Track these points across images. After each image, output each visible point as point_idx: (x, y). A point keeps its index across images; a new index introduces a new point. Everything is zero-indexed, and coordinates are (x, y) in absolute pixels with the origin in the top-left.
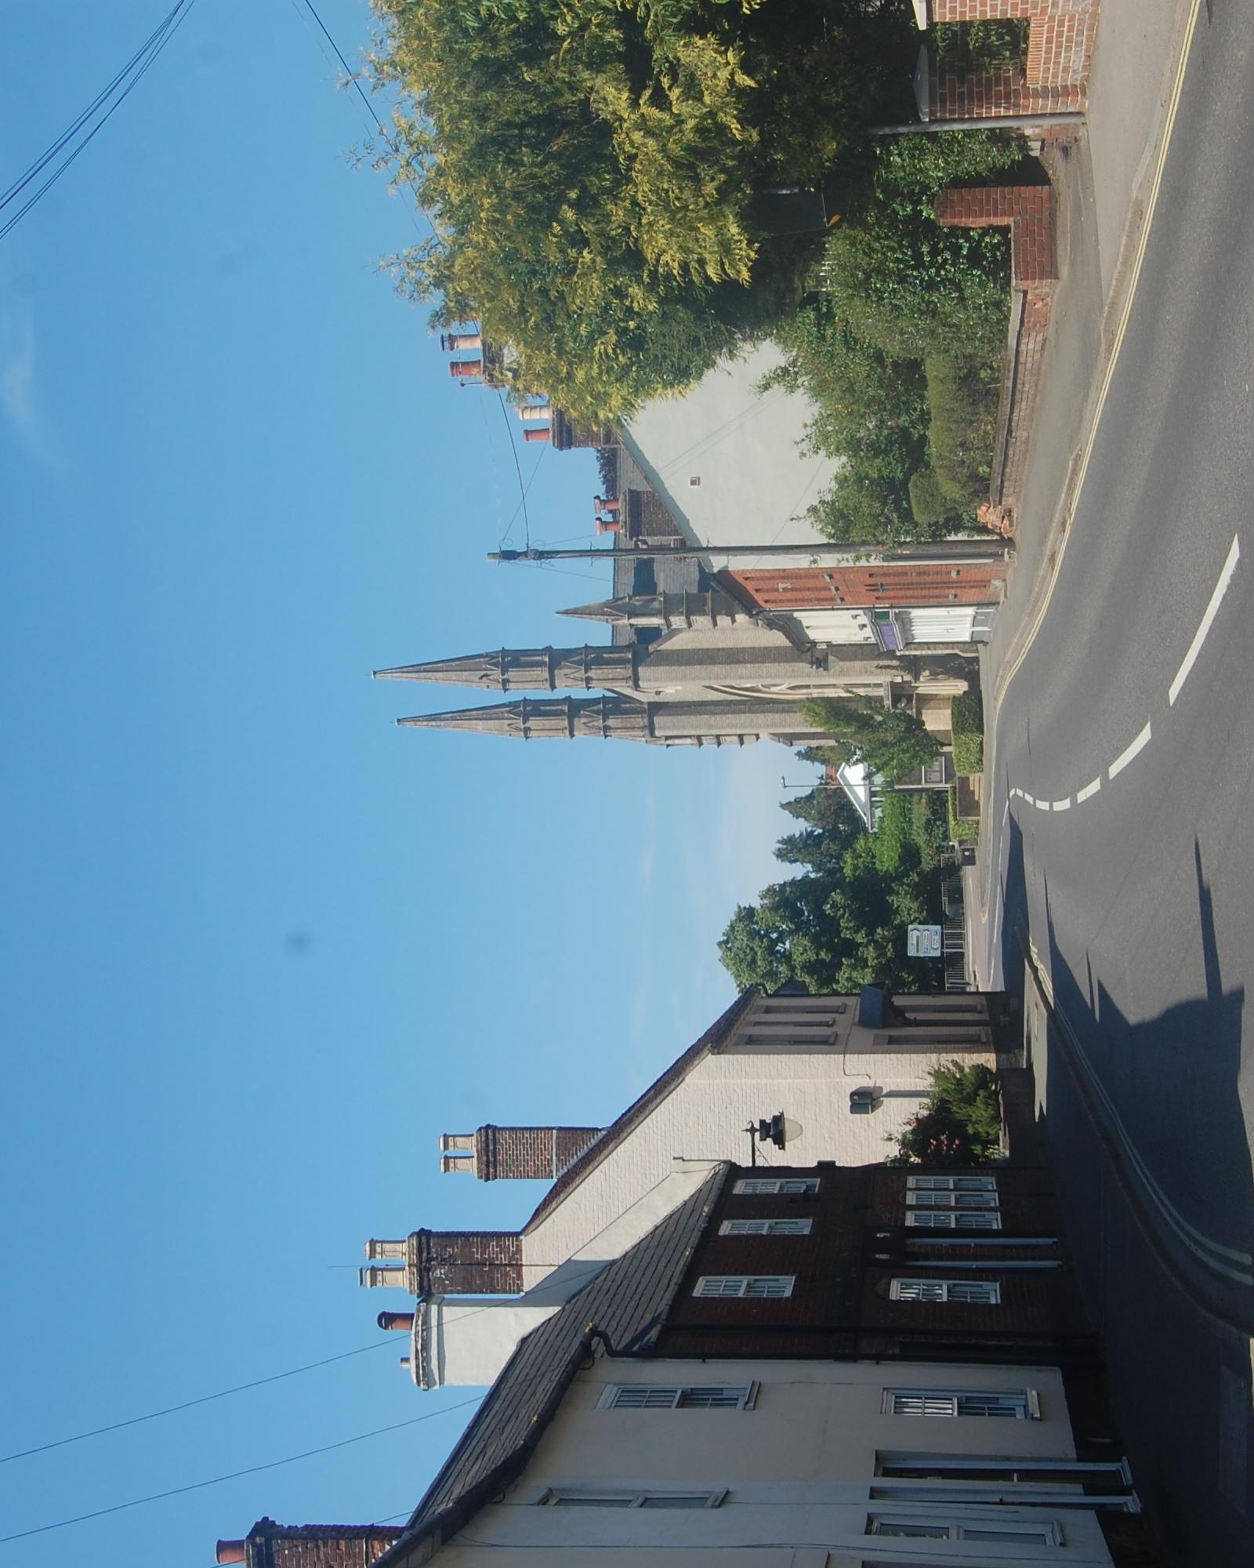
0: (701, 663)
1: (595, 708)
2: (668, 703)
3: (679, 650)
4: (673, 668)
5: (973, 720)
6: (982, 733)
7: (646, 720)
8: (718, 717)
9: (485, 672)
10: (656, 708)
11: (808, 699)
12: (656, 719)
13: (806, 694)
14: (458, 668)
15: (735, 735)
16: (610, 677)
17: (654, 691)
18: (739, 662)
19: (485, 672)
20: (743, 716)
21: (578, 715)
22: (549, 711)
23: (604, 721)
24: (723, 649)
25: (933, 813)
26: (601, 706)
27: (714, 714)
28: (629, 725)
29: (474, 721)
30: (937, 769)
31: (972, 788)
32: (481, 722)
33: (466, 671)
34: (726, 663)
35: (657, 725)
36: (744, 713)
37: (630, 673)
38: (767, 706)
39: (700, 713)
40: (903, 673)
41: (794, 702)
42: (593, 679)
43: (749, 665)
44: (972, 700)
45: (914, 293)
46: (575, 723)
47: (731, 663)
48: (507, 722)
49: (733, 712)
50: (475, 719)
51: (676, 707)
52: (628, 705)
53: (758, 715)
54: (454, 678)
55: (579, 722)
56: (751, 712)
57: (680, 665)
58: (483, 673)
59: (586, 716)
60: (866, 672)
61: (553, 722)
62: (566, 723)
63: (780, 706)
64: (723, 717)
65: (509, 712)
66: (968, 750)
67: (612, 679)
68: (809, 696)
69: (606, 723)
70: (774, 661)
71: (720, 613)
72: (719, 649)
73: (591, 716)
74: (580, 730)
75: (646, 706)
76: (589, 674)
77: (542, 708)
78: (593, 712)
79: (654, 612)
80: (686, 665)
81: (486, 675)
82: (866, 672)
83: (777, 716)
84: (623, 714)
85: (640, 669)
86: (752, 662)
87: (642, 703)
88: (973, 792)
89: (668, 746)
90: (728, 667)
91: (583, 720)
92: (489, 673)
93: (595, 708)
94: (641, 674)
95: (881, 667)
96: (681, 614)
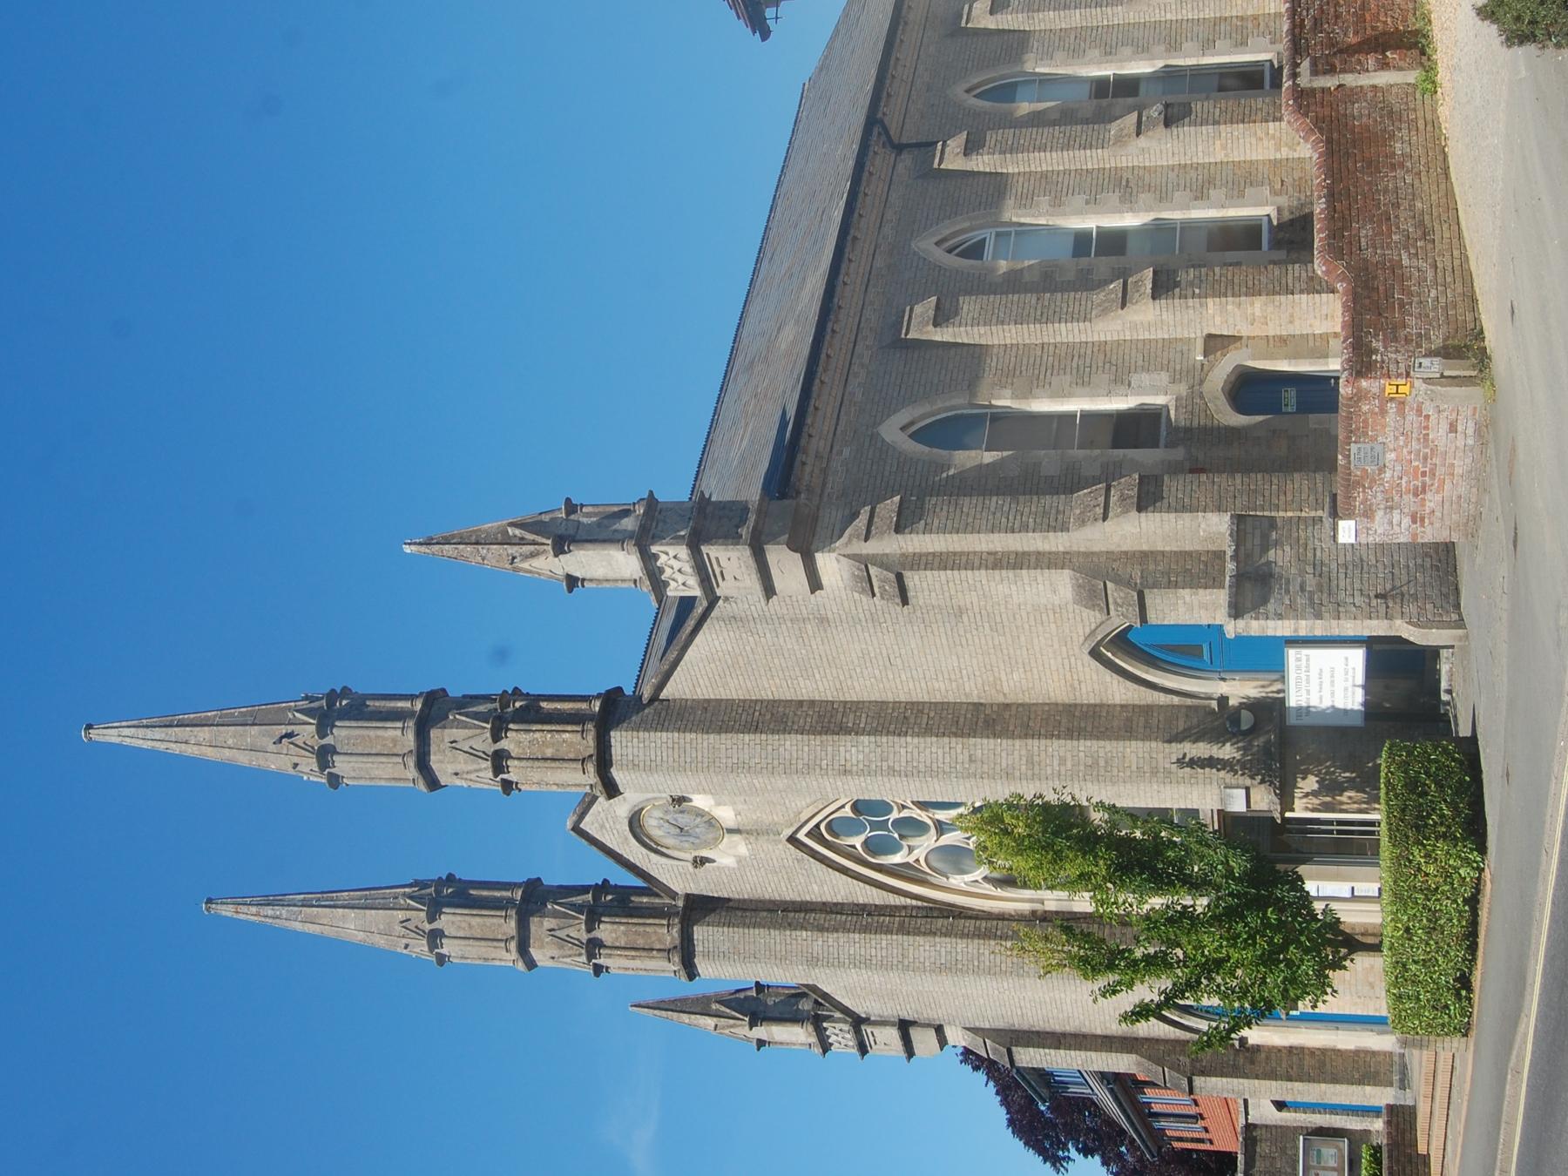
0: (754, 727)
1: (578, 900)
2: (729, 900)
3: (708, 701)
4: (690, 736)
5: (1453, 806)
6: (1482, 850)
7: (675, 931)
8: (832, 938)
9: (290, 729)
10: (700, 908)
11: (1034, 912)
12: (699, 932)
13: (1031, 901)
14: (241, 720)
15: (892, 1024)
16: (549, 752)
17: (690, 857)
18: (842, 730)
19: (290, 729)
20: (884, 940)
21: (540, 911)
22: (486, 898)
23: (589, 930)
24: (812, 703)
25: (1302, 91)
26: (589, 897)
27: (821, 929)
28: (641, 942)
29: (340, 911)
30: (1332, 1163)
31: (1422, 1149)
32: (352, 914)
33: (254, 724)
34: (813, 731)
35: (699, 948)
36: (889, 931)
37: (588, 744)
38: (940, 921)
39: (792, 926)
40: (1248, 782)
41: (1001, 917)
42: (509, 757)
43: (865, 739)
44: (1445, 751)
45: (1455, 889)
46: (533, 928)
47: (826, 731)
48: (401, 915)
49: (865, 929)
50: (344, 907)
51: (745, 910)
52: (645, 900)
53: (920, 939)
54: (230, 742)
55: (540, 926)
56: (903, 930)
57: (707, 730)
58: (284, 729)
59: (556, 915)
60: (1155, 773)
61: (489, 921)
62: (511, 927)
63: (970, 924)
64: (842, 937)
65: (411, 898)
66: (1433, 920)
67: (553, 759)
68: (1038, 907)
69: (596, 934)
70: (927, 731)
71: (773, 539)
72: (801, 703)
73: (566, 916)
74: (542, 947)
75: (680, 903)
76: (504, 744)
77: (472, 892)
78: (573, 906)
79: (620, 536)
80: (720, 731)
81: (289, 735)
82: (1154, 772)
83: (961, 944)
84: (631, 916)
85: (618, 738)
86: (874, 732)
87: (673, 895)
88: (1426, 1159)
89: (761, 1043)
90: (815, 741)
91: (549, 923)
92: (296, 729)
93: (578, 900)
94: (616, 751)
95: (1195, 763)
96: (677, 540)
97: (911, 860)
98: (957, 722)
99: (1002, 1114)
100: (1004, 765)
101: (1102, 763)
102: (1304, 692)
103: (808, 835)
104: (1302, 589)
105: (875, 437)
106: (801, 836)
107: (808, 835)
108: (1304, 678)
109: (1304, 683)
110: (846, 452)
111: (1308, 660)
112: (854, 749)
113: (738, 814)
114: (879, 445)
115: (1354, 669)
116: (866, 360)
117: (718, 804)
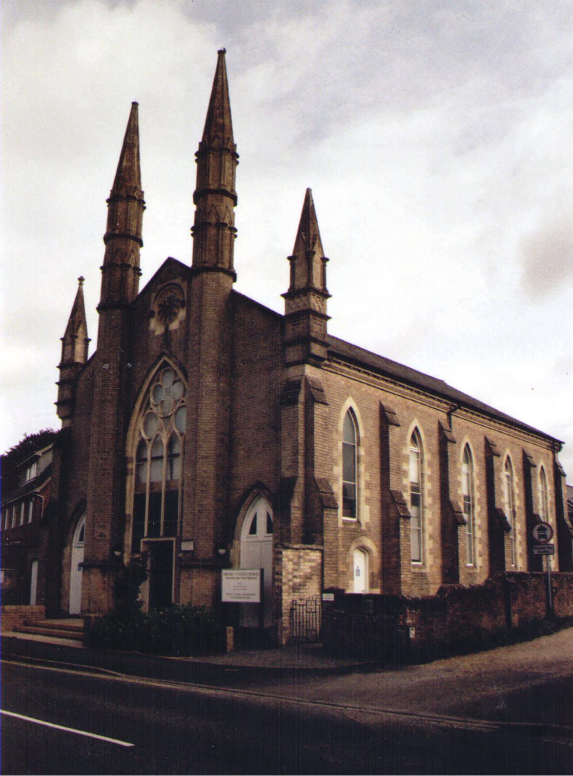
97: (151, 406)
98: (293, 423)
99: (192, 223)
100: (329, 522)
101: (204, 489)
102: (238, 576)
103: (165, 361)
104: (295, 577)
105: (348, 395)
106: (165, 358)
107: (165, 361)
108: (245, 576)
109: (242, 576)
110: (343, 382)
111: (254, 578)
112: (211, 380)
113: (175, 330)
114: (345, 397)
115: (249, 598)
116: (376, 394)
117: (180, 322)
